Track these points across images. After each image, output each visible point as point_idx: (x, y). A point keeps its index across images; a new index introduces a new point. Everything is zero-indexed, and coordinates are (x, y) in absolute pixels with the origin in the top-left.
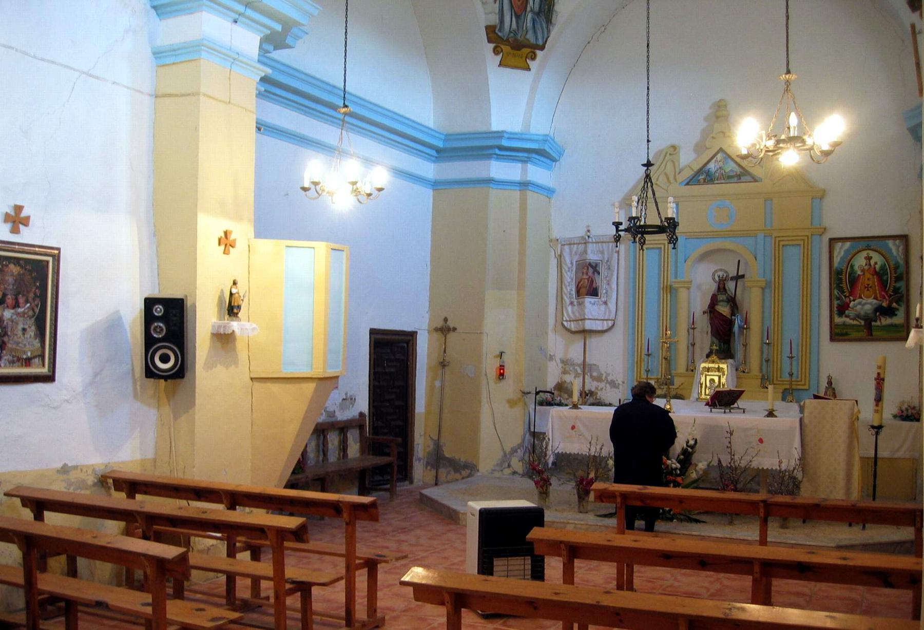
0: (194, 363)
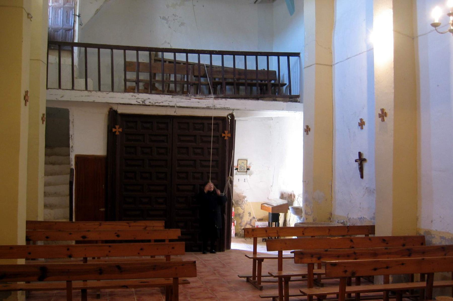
0: (288, 109)
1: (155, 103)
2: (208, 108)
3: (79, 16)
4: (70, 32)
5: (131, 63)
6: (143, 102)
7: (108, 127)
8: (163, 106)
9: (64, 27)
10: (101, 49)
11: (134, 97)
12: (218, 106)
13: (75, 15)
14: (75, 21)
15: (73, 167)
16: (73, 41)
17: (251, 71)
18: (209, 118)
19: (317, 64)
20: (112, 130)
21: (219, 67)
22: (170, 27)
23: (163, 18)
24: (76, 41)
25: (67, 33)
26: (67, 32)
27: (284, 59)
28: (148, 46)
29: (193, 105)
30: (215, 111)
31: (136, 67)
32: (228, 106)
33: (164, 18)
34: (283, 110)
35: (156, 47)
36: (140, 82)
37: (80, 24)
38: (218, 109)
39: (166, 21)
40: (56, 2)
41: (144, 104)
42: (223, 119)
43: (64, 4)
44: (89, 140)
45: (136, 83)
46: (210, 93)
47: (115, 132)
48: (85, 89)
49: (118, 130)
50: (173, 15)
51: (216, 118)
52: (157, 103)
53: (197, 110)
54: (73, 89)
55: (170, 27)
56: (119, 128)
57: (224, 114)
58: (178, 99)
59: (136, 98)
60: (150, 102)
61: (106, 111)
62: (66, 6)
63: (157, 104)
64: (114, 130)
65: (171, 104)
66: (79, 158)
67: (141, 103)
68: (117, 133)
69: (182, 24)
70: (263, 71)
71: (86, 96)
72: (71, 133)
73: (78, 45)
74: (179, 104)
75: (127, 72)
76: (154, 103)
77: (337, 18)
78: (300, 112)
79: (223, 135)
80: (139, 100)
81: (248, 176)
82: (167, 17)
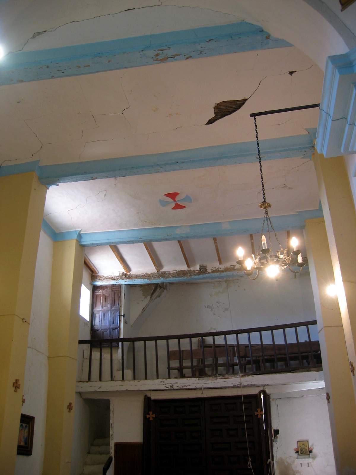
1: (183, 387)
2: (235, 387)
3: (124, 316)
4: (116, 331)
5: (174, 352)
6: (171, 387)
7: (144, 414)
8: (191, 389)
9: (112, 326)
10: (146, 342)
11: (162, 383)
12: (245, 384)
13: (120, 315)
14: (120, 321)
15: (113, 455)
16: (119, 337)
18: (238, 397)
19: (325, 327)
20: (146, 417)
21: (258, 345)
23: (207, 307)
24: (121, 337)
25: (114, 332)
29: (219, 385)
30: (245, 389)
31: (179, 355)
32: (255, 383)
33: (208, 307)
34: (315, 380)
36: (183, 369)
37: (125, 323)
38: (244, 387)
39: (210, 309)
40: (105, 307)
41: (172, 388)
42: (256, 397)
44: (127, 427)
45: (179, 370)
46: (183, 351)
47: (149, 418)
48: (110, 379)
49: (151, 416)
50: (217, 302)
51: (247, 397)
52: (185, 386)
53: (227, 390)
54: (112, 380)
56: (152, 414)
57: (254, 391)
58: (204, 380)
59: (165, 383)
60: (178, 387)
61: (141, 399)
62: (113, 308)
63: (184, 388)
64: (148, 416)
65: (198, 386)
66: (118, 446)
67: (170, 388)
68: (151, 419)
69: (226, 309)
70: (305, 343)
71: (120, 386)
72: (111, 422)
73: (123, 340)
74: (205, 386)
75: (170, 361)
76: (181, 387)
78: (322, 381)
79: (256, 413)
80: (167, 386)
81: (310, 460)
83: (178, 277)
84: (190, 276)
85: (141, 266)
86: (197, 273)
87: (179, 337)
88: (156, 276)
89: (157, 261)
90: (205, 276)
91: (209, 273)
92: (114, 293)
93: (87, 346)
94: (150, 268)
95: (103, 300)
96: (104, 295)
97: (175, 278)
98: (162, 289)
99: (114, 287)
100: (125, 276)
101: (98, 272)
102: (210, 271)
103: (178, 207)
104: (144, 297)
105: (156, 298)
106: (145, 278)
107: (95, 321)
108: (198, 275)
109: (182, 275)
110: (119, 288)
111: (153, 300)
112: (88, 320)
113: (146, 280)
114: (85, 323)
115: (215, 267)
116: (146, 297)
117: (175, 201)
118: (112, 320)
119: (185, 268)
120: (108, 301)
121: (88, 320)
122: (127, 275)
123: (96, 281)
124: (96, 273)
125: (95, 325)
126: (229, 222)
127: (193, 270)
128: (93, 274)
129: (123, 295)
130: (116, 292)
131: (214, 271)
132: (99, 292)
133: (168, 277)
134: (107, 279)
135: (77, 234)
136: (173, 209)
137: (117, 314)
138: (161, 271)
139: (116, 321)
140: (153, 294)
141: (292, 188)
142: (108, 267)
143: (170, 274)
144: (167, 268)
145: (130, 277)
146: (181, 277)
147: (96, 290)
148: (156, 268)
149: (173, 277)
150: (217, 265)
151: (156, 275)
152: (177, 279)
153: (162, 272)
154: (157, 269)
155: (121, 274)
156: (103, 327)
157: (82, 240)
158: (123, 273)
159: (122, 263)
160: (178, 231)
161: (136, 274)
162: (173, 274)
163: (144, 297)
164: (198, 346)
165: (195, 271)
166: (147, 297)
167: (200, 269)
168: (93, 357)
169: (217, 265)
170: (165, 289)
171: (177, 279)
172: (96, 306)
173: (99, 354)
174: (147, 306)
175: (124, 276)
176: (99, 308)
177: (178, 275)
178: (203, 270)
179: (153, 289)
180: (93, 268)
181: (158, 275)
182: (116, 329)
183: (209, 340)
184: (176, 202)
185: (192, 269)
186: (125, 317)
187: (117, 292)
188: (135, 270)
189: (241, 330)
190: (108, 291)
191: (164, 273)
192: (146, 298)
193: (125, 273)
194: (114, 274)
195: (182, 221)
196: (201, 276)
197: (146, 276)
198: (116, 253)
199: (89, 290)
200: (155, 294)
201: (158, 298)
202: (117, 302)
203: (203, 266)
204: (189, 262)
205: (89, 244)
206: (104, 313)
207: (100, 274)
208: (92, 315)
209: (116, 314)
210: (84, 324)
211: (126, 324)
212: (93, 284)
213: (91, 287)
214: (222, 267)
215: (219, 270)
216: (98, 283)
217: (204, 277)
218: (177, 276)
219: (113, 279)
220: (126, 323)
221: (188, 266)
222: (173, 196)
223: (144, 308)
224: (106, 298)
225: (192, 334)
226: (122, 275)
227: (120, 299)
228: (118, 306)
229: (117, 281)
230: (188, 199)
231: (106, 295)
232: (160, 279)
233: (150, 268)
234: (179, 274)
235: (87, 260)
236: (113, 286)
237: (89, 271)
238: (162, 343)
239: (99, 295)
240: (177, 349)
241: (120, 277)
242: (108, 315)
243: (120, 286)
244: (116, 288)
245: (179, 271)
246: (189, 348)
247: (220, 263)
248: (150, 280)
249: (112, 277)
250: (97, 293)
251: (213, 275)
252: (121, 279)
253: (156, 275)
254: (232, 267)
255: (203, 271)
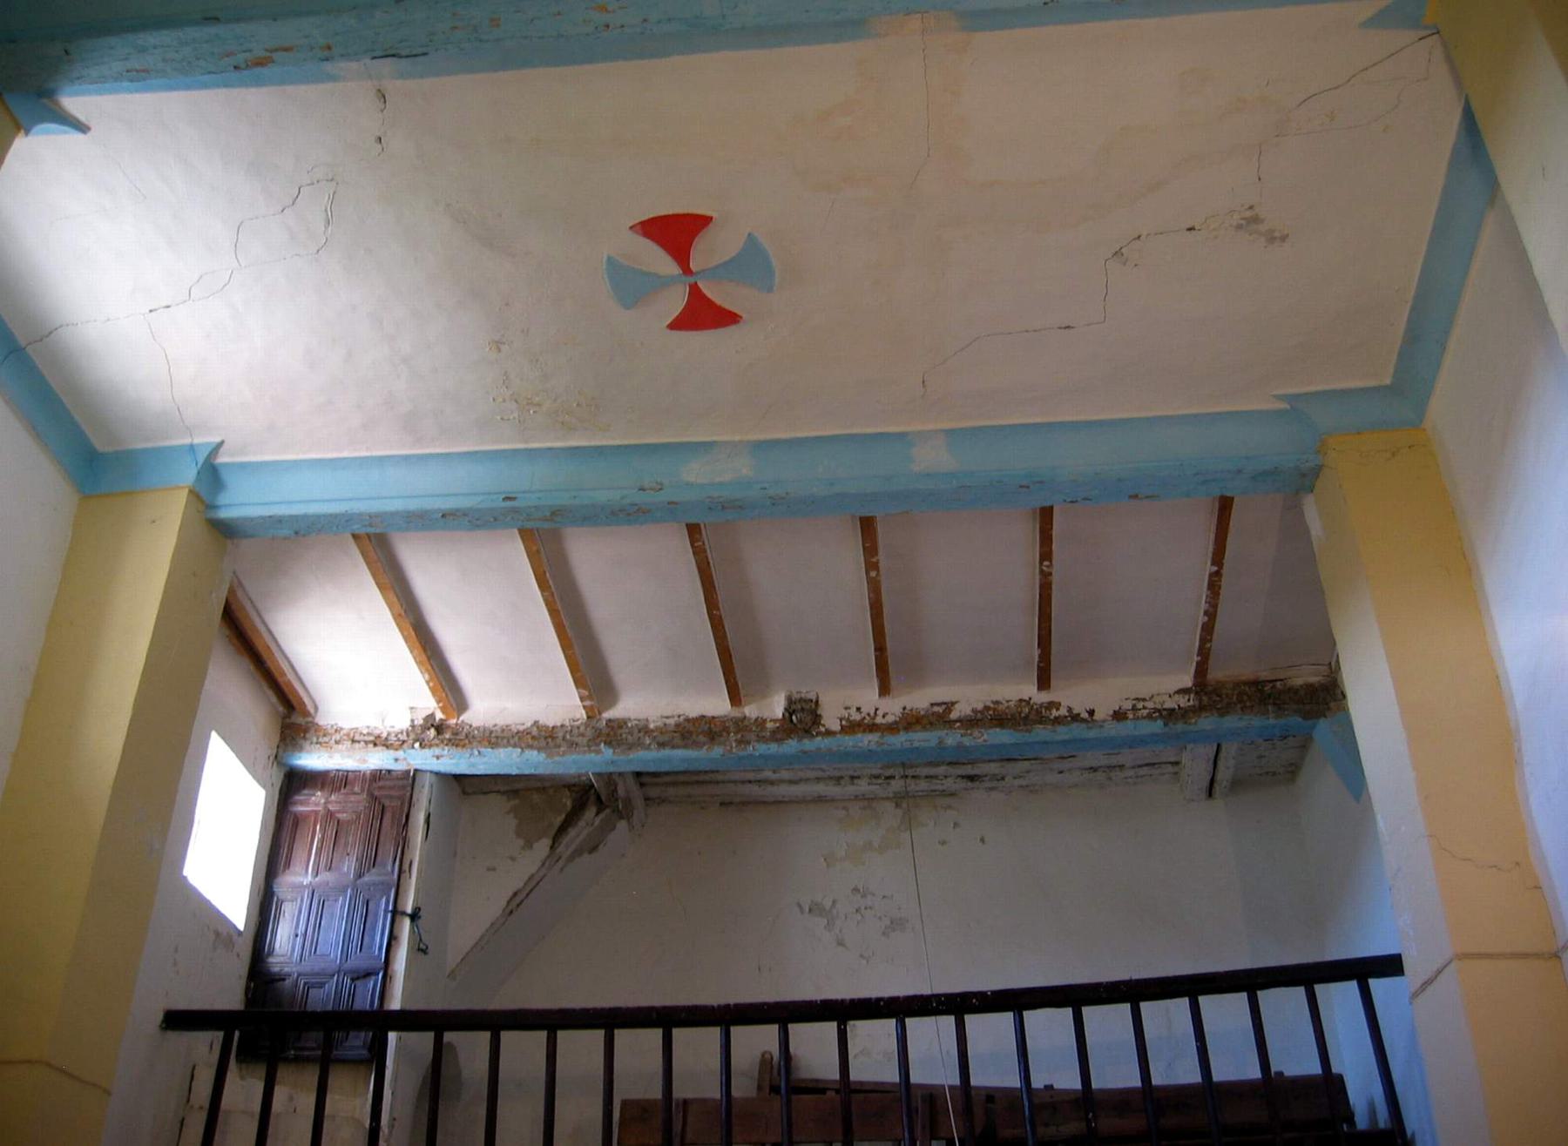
3: (414, 917)
9: (352, 963)
14: (393, 938)
17: (1237, 1091)
22: (841, 943)
24: (395, 1004)
26: (358, 983)
27: (1340, 998)
28: (732, 1001)
33: (815, 909)
35: (732, 1000)
37: (420, 949)
43: (360, 875)
46: (685, 1102)
50: (856, 890)
55: (841, 943)
62: (366, 878)
69: (897, 924)
73: (408, 1020)
77: (1519, 701)
82: (828, 904)
83: (685, 747)
84: (739, 742)
85: (518, 687)
86: (774, 732)
87: (667, 1019)
88: (579, 740)
89: (591, 672)
90: (808, 744)
91: (829, 733)
92: (378, 808)
93: (204, 1046)
94: (561, 703)
95: (322, 841)
96: (330, 815)
97: (667, 752)
98: (608, 811)
99: (381, 783)
100: (435, 731)
101: (316, 708)
102: (836, 727)
103: (702, 314)
104: (521, 842)
105: (578, 853)
106: (531, 747)
107: (274, 933)
108: (779, 741)
109: (702, 738)
110: (404, 787)
111: (560, 864)
112: (241, 927)
113: (535, 752)
114: (217, 934)
115: (858, 709)
116: (529, 845)
117: (687, 271)
118: (356, 935)
119: (717, 704)
120: (346, 844)
121: (241, 927)
122: (448, 727)
123: (301, 749)
124: (306, 714)
125: (271, 952)
126: (949, 433)
127: (754, 716)
128: (291, 715)
129: (419, 818)
130: (387, 803)
131: (851, 727)
132: (313, 802)
133: (638, 744)
134: (353, 741)
135: (201, 461)
136: (674, 326)
137: (383, 905)
138: (607, 715)
139: (373, 939)
140: (562, 829)
141: (1284, 238)
142: (358, 675)
143: (644, 729)
144: (637, 704)
145: (461, 738)
146: (697, 745)
147: (298, 790)
148: (582, 699)
149: (662, 745)
150: (867, 698)
151: (583, 735)
152: (680, 753)
153: (610, 721)
154: (588, 703)
155: (419, 722)
156: (306, 967)
157: (223, 499)
158: (432, 716)
159: (424, 658)
160: (696, 474)
161: (490, 724)
162: (662, 730)
163: (521, 842)
164: (760, 1088)
165: (764, 721)
166: (535, 845)
167: (790, 711)
168: (226, 1102)
169: (867, 698)
170: (622, 818)
171: (679, 757)
172: (288, 864)
173: (259, 1087)
174: (533, 884)
175: (432, 732)
176: (300, 877)
177: (683, 737)
178: (803, 717)
179: (570, 806)
180: (289, 684)
181: (589, 733)
182: (368, 974)
183: (814, 1048)
184: (692, 280)
185: (750, 711)
186: (420, 922)
187: (397, 803)
188: (483, 709)
189: (981, 995)
190: (353, 798)
191: (617, 725)
192: (531, 847)
193: (439, 715)
194: (388, 723)
195: (714, 409)
196: (791, 746)
197: (533, 738)
198: (392, 595)
199: (264, 787)
200: (572, 832)
201: (586, 857)
202: (388, 849)
203: (801, 700)
204: (738, 672)
205: (252, 519)
206: (319, 900)
207: (323, 720)
208: (265, 904)
209: (378, 906)
210: (212, 937)
211: (421, 955)
212: (284, 765)
213: (277, 778)
214: (892, 708)
215: (879, 720)
216: (312, 759)
217: (805, 752)
218: (678, 741)
219: (379, 742)
220: (424, 952)
221: (735, 697)
222: (676, 233)
223: (515, 894)
224: (337, 830)
225: (736, 1005)
226: (425, 728)
227: (405, 839)
228: (389, 868)
229: (400, 754)
230: (752, 263)
231: (339, 816)
232: (598, 752)
233: (561, 703)
234: (691, 733)
235: (240, 594)
236: (378, 776)
237: (274, 699)
238: (579, 1048)
239: (306, 816)
240: (656, 1093)
241: (412, 736)
242: (338, 911)
243: (411, 779)
244: (391, 788)
245: (688, 720)
246: (714, 1092)
247: (884, 690)
248: (549, 755)
249: (377, 732)
250: (302, 803)
251: (849, 741)
252: (417, 745)
253: (583, 735)
254: (936, 709)
255: (800, 721)
